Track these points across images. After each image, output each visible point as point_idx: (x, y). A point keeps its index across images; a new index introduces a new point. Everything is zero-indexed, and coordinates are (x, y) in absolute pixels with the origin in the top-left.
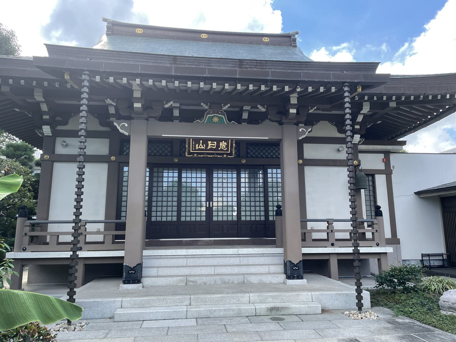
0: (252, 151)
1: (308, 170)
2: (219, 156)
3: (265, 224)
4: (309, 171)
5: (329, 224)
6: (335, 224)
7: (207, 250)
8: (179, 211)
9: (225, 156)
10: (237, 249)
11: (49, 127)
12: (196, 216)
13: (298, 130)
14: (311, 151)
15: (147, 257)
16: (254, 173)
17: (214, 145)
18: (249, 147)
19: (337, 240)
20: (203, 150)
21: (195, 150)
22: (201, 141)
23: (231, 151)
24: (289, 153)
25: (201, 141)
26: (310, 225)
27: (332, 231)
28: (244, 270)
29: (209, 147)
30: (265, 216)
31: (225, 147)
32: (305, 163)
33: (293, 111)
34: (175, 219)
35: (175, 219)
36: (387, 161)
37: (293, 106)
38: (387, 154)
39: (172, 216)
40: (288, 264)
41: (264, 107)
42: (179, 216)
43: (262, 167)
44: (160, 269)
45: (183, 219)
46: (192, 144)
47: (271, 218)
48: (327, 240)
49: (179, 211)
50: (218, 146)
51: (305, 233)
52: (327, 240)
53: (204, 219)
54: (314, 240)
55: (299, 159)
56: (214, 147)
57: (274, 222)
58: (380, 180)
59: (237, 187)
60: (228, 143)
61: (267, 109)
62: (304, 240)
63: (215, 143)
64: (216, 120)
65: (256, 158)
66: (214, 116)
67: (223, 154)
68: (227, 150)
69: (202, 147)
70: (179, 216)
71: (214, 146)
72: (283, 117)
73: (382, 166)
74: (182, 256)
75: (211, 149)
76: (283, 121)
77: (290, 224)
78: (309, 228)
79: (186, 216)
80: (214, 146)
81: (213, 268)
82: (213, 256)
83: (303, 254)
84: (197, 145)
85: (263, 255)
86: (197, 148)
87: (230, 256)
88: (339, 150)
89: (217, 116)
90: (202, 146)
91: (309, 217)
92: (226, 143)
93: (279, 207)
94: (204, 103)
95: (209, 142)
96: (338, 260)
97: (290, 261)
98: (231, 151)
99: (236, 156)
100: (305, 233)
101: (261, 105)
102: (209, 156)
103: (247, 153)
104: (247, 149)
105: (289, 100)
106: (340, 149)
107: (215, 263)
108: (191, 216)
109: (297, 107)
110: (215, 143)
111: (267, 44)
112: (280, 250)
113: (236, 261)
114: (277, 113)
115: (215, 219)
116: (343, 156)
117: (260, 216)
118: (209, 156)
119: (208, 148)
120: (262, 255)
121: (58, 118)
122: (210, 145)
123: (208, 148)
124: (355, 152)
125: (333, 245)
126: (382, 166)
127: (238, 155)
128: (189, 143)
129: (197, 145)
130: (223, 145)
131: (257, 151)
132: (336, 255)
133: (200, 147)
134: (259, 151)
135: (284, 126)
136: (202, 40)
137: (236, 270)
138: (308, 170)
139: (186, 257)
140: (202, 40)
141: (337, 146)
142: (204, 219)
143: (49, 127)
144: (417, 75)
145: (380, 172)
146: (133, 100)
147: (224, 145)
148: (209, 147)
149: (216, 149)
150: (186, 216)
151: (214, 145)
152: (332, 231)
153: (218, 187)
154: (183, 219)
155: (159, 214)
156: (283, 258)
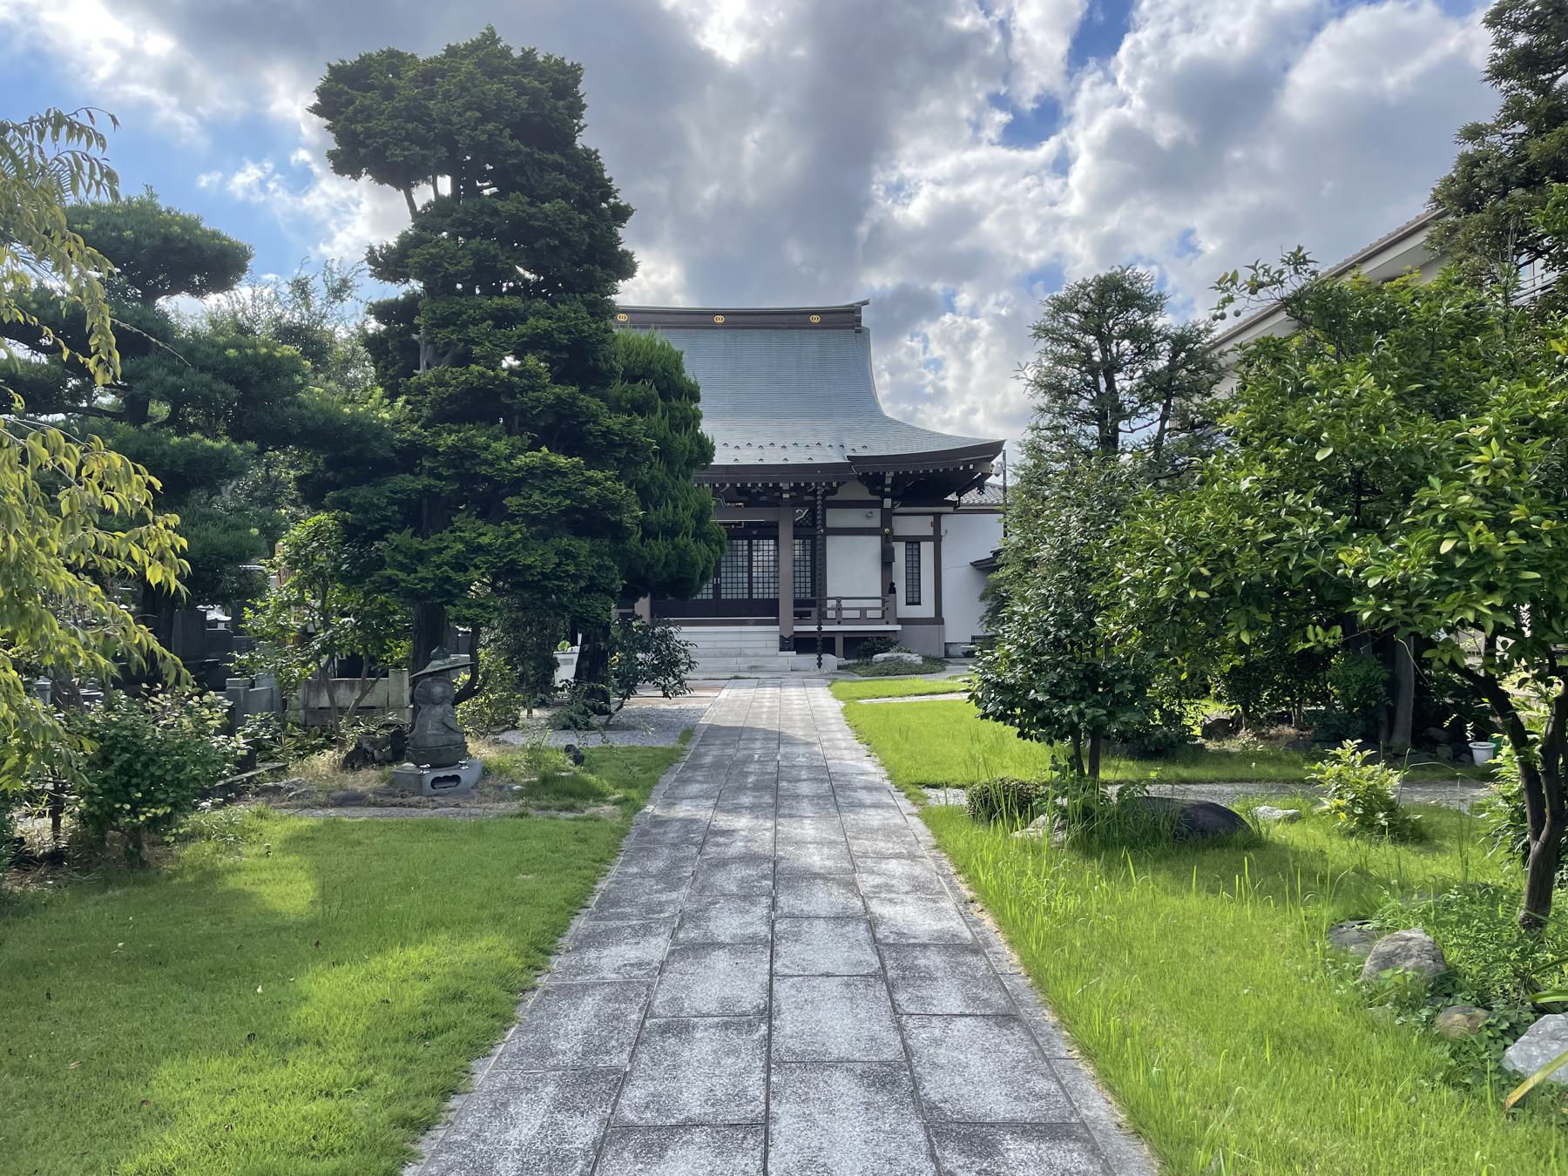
28: (742, 645)
36: (937, 525)
38: (937, 516)
42: (750, 593)
58: (927, 549)
70: (750, 593)
73: (930, 532)
111: (815, 327)
112: (776, 628)
113: (733, 637)
116: (875, 522)
124: (887, 517)
126: (930, 532)
136: (717, 327)
137: (735, 645)
140: (717, 327)
144: (190, 225)
145: (927, 538)
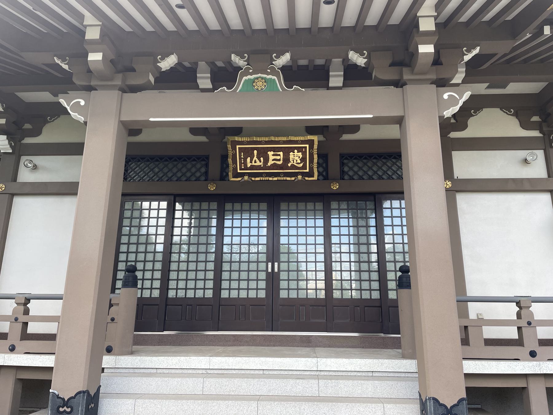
0: (351, 169)
1: (462, 200)
2: (288, 179)
3: (381, 307)
4: (465, 202)
5: (520, 308)
6: (33, 306)
7: (252, 359)
8: (218, 280)
9: (300, 177)
10: (314, 360)
11: (5, 137)
12: (248, 289)
13: (439, 97)
14: (467, 165)
15: (131, 371)
16: (357, 209)
17: (278, 158)
18: (345, 161)
19: (544, 343)
20: (259, 168)
21: (246, 168)
22: (255, 152)
23: (311, 169)
24: (422, 149)
25: (255, 152)
26: (475, 310)
27: (529, 323)
29: (270, 163)
30: (380, 290)
31: (299, 161)
32: (457, 187)
33: (426, 49)
34: (209, 294)
35: (209, 294)
37: (427, 36)
39: (204, 289)
40: (430, 406)
41: (362, 54)
42: (217, 288)
43: (372, 198)
44: (140, 402)
45: (224, 294)
46: (240, 158)
47: (392, 295)
48: (519, 342)
49: (218, 280)
50: (286, 159)
51: (466, 327)
52: (519, 342)
53: (262, 294)
54: (490, 342)
55: (446, 179)
56: (280, 163)
57: (396, 301)
59: (324, 236)
60: (304, 154)
61: (369, 57)
62: (465, 342)
63: (281, 153)
64: (260, 85)
65: (357, 175)
66: (257, 78)
67: (295, 175)
68: (304, 167)
69: (258, 163)
70: (217, 288)
71: (279, 160)
72: (405, 70)
74: (200, 372)
75: (274, 166)
76: (406, 77)
77: (429, 309)
78: (472, 316)
79: (230, 289)
80: (279, 160)
81: (254, 404)
82: (265, 374)
83: (465, 374)
84: (249, 160)
85: (371, 376)
86: (249, 165)
87: (300, 375)
88: (526, 161)
89: (262, 78)
90: (257, 160)
91: (472, 291)
92: (300, 154)
93: (405, 270)
94: (237, 54)
95: (270, 153)
96: (547, 389)
97: (435, 400)
98: (311, 169)
99: (321, 178)
100: (466, 327)
101: (356, 52)
102: (271, 179)
103: (343, 173)
104: (342, 164)
105: (417, 26)
106: (529, 158)
107: (264, 391)
108: (239, 289)
109: (436, 38)
110: (281, 153)
112: (410, 365)
113: (310, 387)
114: (392, 65)
115: (283, 294)
117: (370, 290)
118: (271, 179)
119: (269, 164)
120: (370, 374)
121: (27, 126)
122: (271, 157)
123: (269, 164)
125: (533, 354)
127: (325, 176)
128: (234, 156)
129: (249, 160)
130: (295, 157)
131: (360, 168)
132: (543, 379)
133: (253, 164)
134: (365, 169)
135: (407, 88)
138: (462, 200)
139: (207, 373)
141: (522, 154)
142: (262, 294)
143: (5, 137)
146: (87, 47)
147: (297, 158)
148: (270, 163)
149: (284, 166)
150: (230, 289)
151: (278, 158)
152: (529, 323)
153: (306, 244)
154: (224, 294)
155: (182, 284)
156: (417, 389)
